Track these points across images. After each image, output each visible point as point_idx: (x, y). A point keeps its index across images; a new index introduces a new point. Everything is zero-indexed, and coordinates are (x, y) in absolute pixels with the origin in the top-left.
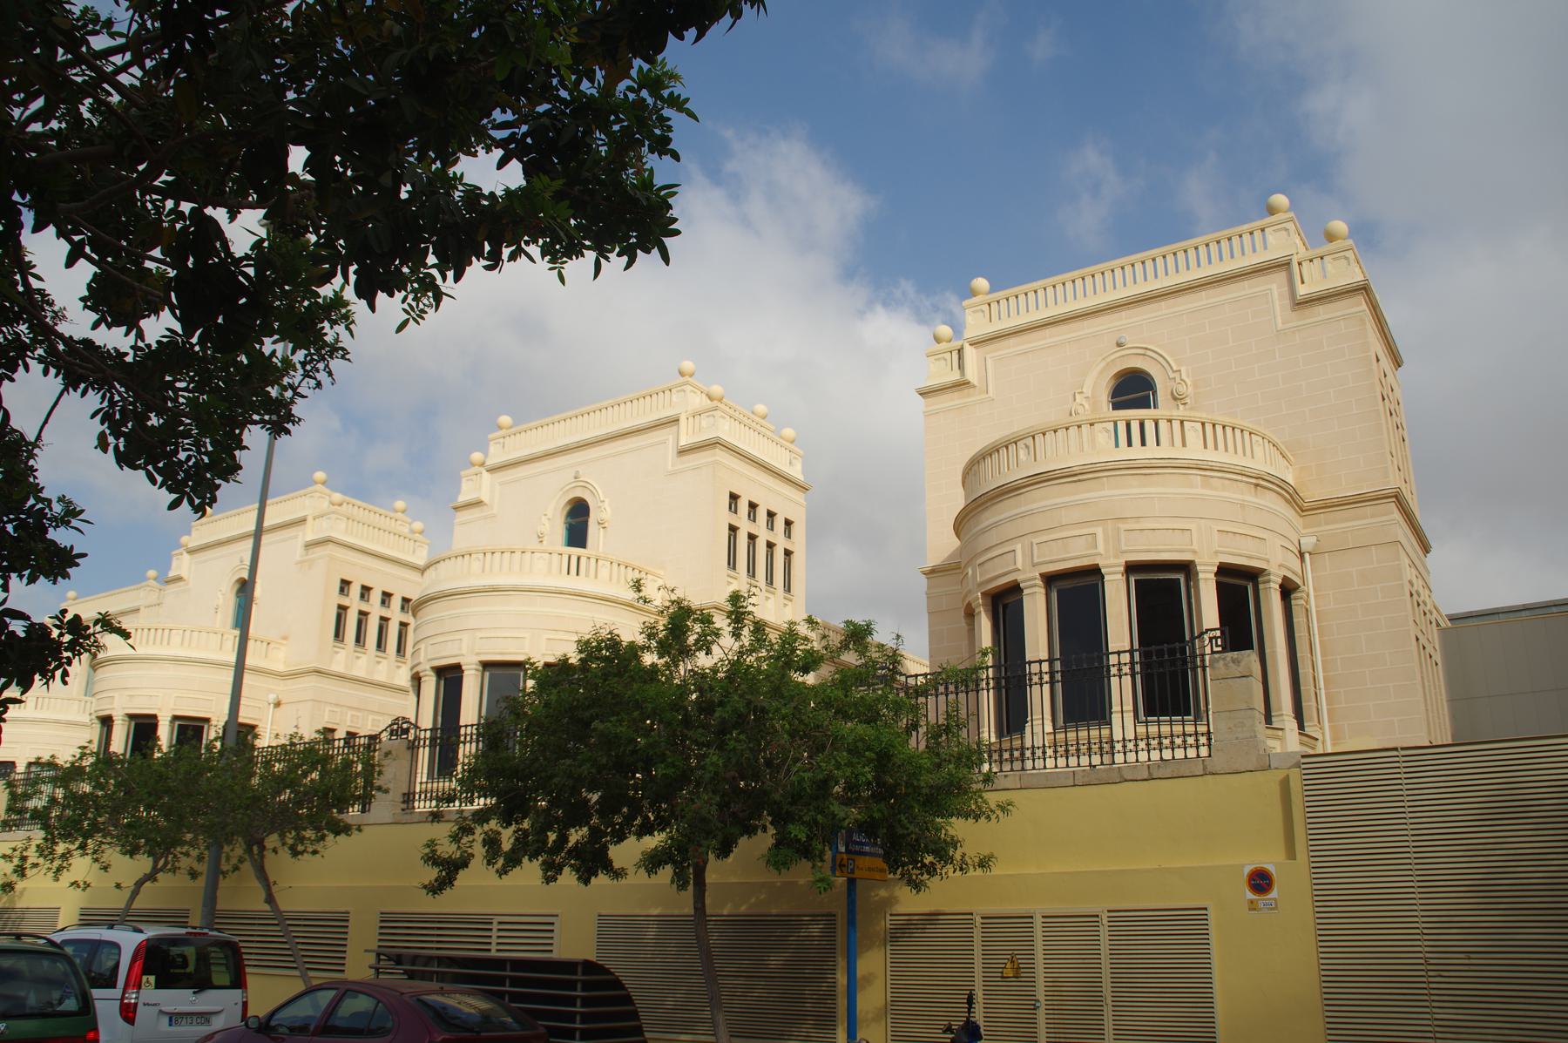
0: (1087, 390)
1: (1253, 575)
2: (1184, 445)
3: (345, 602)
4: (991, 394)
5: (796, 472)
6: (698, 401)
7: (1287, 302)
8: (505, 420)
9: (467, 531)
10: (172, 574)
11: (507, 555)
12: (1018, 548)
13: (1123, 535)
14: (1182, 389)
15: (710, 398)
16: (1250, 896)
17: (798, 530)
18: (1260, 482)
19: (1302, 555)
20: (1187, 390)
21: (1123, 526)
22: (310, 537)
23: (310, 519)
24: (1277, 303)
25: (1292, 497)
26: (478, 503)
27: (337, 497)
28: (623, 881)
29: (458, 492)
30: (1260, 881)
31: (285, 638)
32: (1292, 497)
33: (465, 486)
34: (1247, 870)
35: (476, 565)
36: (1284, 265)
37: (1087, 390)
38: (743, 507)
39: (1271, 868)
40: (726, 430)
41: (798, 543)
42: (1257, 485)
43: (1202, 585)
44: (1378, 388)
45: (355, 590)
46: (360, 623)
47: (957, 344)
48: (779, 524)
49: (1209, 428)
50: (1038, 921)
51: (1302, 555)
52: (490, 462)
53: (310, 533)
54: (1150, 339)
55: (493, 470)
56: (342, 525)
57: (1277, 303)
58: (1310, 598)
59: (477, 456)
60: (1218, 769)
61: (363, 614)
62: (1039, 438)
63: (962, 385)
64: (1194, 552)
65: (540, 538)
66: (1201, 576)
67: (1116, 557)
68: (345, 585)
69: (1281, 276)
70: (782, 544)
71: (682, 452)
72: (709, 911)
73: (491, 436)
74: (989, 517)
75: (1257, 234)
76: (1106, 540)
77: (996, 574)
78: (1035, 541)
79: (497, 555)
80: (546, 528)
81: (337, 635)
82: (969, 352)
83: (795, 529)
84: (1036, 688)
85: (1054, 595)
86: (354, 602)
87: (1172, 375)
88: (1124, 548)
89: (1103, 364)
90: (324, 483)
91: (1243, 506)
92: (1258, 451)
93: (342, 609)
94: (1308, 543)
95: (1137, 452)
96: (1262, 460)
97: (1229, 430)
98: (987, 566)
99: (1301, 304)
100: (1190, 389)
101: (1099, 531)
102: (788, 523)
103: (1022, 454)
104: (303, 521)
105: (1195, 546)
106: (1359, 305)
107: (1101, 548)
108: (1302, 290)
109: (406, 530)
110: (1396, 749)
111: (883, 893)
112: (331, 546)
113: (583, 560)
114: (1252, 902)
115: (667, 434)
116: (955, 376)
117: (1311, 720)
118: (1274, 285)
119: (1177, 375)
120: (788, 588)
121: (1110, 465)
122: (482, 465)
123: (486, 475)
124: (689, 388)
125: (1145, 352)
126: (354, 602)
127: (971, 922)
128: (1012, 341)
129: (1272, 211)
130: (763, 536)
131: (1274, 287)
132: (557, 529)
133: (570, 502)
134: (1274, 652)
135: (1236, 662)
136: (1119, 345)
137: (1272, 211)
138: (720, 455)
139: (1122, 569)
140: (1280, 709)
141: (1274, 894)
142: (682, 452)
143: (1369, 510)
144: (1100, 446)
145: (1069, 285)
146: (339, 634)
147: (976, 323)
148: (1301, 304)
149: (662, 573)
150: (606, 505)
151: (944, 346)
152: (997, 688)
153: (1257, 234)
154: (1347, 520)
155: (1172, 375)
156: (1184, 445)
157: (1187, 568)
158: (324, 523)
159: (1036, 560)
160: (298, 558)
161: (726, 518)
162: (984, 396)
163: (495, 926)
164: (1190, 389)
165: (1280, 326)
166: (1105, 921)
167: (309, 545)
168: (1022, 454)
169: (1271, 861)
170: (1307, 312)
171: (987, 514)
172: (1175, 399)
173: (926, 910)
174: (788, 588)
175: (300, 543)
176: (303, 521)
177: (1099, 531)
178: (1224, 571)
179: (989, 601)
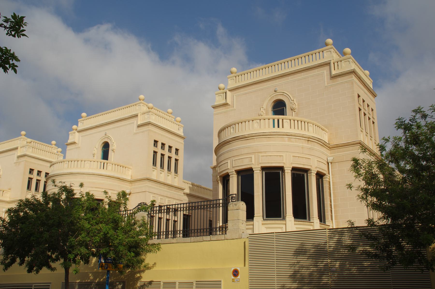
0: (265, 107)
1: (306, 171)
2: (283, 127)
3: (31, 176)
4: (235, 108)
5: (181, 133)
6: (145, 109)
7: (329, 76)
8: (84, 114)
9: (71, 152)
10: (69, 141)
11: (76, 162)
12: (229, 161)
13: (260, 157)
14: (294, 106)
15: (149, 108)
16: (233, 277)
17: (181, 152)
18: (309, 139)
19: (328, 163)
20: (296, 107)
21: (261, 155)
22: (19, 154)
23: (19, 148)
24: (326, 77)
25: (323, 144)
26: (74, 143)
27: (29, 140)
28: (55, 272)
29: (68, 139)
30: (236, 273)
31: (10, 189)
32: (323, 144)
33: (70, 137)
34: (233, 269)
35: (66, 166)
36: (328, 64)
37: (265, 107)
38: (159, 145)
39: (239, 269)
40: (153, 119)
41: (181, 156)
42: (308, 140)
43: (286, 174)
44: (358, 106)
45: (35, 172)
46: (37, 184)
47: (225, 90)
48: (173, 150)
49: (292, 121)
50: (177, 284)
51: (328, 163)
52: (79, 129)
53: (19, 152)
54: (287, 90)
55: (79, 132)
56: (31, 150)
57: (326, 77)
58: (329, 179)
59: (75, 127)
60: (228, 238)
61: (163, 155)
62: (70, 162)
63: (226, 105)
64: (284, 163)
65: (94, 155)
66: (286, 171)
67: (258, 165)
68: (31, 171)
69: (327, 68)
70: (174, 156)
71: (139, 126)
72: (70, 281)
73: (79, 120)
74: (222, 151)
75: (321, 53)
76: (255, 159)
77: (222, 170)
78: (234, 159)
79: (73, 162)
80: (95, 151)
81: (153, 164)
82: (229, 93)
83: (374, 111)
84: (179, 212)
85: (240, 177)
86: (35, 176)
87: (291, 102)
88: (260, 162)
89: (270, 97)
90: (25, 135)
91: (303, 148)
92: (311, 129)
93: (30, 179)
94: (330, 159)
95: (276, 130)
96: (312, 132)
97: (299, 122)
98: (221, 167)
99: (333, 77)
100: (297, 107)
101: (253, 156)
102: (177, 150)
103: (232, 130)
104: (17, 148)
105: (284, 161)
106: (353, 78)
107: (253, 162)
108: (334, 72)
109: (56, 151)
110: (273, 233)
111: (138, 275)
112: (26, 157)
113: (105, 164)
114: (233, 279)
115: (133, 120)
116: (224, 102)
117: (328, 219)
118: (325, 71)
119: (293, 102)
120: (176, 171)
121: (257, 134)
122: (76, 130)
123: (77, 133)
124: (142, 104)
125: (283, 94)
126: (35, 176)
127: (160, 284)
128: (242, 90)
129: (326, 45)
130: (167, 154)
131: (325, 71)
132: (99, 153)
133: (103, 143)
134: (312, 197)
135: (236, 205)
136: (275, 91)
137: (326, 45)
138: (151, 128)
139: (260, 169)
140: (313, 216)
141: (239, 277)
142: (139, 126)
143: (351, 148)
144: (267, 127)
145: (317, 54)
146: (154, 163)
147: (232, 84)
148: (333, 77)
149: (131, 167)
150: (115, 144)
151: (222, 91)
152: (223, 207)
153: (321, 53)
154: (344, 151)
155: (291, 102)
156: (283, 127)
157: (282, 168)
158: (24, 149)
159: (234, 166)
160: (15, 161)
161: (28, 175)
162: (233, 108)
163: (33, 286)
164: (297, 107)
165: (326, 85)
166: (195, 285)
167: (19, 157)
168: (232, 130)
169: (239, 267)
170: (335, 80)
171: (221, 150)
172: (292, 110)
173: (149, 280)
174: (176, 171)
175: (16, 156)
176: (17, 148)
177: (253, 156)
178: (294, 169)
179: (222, 178)
